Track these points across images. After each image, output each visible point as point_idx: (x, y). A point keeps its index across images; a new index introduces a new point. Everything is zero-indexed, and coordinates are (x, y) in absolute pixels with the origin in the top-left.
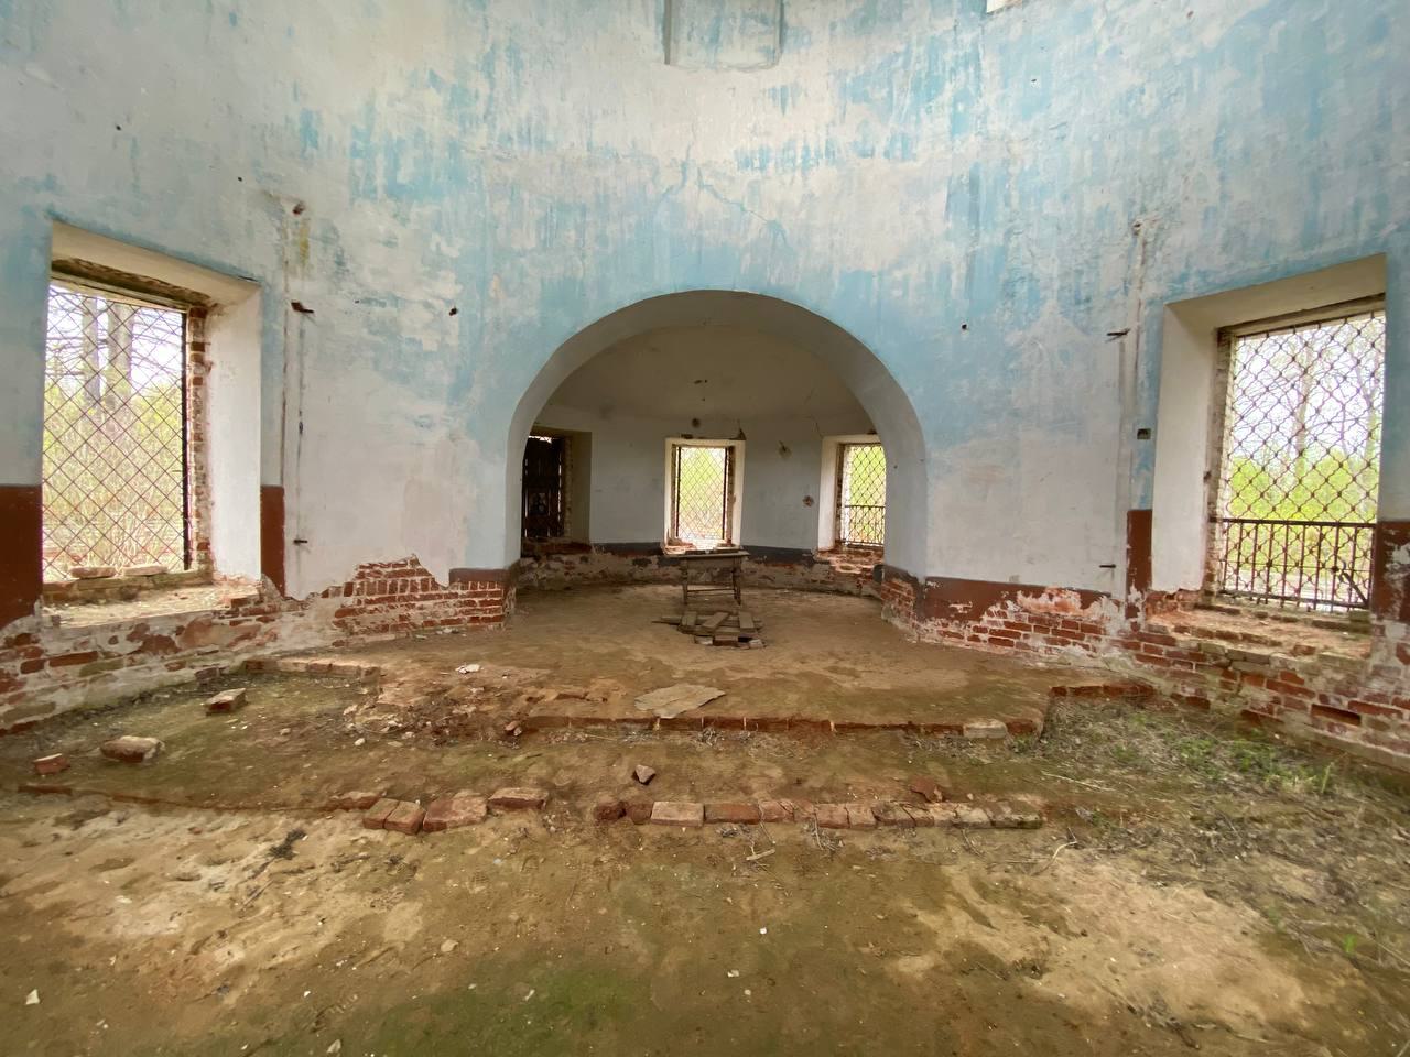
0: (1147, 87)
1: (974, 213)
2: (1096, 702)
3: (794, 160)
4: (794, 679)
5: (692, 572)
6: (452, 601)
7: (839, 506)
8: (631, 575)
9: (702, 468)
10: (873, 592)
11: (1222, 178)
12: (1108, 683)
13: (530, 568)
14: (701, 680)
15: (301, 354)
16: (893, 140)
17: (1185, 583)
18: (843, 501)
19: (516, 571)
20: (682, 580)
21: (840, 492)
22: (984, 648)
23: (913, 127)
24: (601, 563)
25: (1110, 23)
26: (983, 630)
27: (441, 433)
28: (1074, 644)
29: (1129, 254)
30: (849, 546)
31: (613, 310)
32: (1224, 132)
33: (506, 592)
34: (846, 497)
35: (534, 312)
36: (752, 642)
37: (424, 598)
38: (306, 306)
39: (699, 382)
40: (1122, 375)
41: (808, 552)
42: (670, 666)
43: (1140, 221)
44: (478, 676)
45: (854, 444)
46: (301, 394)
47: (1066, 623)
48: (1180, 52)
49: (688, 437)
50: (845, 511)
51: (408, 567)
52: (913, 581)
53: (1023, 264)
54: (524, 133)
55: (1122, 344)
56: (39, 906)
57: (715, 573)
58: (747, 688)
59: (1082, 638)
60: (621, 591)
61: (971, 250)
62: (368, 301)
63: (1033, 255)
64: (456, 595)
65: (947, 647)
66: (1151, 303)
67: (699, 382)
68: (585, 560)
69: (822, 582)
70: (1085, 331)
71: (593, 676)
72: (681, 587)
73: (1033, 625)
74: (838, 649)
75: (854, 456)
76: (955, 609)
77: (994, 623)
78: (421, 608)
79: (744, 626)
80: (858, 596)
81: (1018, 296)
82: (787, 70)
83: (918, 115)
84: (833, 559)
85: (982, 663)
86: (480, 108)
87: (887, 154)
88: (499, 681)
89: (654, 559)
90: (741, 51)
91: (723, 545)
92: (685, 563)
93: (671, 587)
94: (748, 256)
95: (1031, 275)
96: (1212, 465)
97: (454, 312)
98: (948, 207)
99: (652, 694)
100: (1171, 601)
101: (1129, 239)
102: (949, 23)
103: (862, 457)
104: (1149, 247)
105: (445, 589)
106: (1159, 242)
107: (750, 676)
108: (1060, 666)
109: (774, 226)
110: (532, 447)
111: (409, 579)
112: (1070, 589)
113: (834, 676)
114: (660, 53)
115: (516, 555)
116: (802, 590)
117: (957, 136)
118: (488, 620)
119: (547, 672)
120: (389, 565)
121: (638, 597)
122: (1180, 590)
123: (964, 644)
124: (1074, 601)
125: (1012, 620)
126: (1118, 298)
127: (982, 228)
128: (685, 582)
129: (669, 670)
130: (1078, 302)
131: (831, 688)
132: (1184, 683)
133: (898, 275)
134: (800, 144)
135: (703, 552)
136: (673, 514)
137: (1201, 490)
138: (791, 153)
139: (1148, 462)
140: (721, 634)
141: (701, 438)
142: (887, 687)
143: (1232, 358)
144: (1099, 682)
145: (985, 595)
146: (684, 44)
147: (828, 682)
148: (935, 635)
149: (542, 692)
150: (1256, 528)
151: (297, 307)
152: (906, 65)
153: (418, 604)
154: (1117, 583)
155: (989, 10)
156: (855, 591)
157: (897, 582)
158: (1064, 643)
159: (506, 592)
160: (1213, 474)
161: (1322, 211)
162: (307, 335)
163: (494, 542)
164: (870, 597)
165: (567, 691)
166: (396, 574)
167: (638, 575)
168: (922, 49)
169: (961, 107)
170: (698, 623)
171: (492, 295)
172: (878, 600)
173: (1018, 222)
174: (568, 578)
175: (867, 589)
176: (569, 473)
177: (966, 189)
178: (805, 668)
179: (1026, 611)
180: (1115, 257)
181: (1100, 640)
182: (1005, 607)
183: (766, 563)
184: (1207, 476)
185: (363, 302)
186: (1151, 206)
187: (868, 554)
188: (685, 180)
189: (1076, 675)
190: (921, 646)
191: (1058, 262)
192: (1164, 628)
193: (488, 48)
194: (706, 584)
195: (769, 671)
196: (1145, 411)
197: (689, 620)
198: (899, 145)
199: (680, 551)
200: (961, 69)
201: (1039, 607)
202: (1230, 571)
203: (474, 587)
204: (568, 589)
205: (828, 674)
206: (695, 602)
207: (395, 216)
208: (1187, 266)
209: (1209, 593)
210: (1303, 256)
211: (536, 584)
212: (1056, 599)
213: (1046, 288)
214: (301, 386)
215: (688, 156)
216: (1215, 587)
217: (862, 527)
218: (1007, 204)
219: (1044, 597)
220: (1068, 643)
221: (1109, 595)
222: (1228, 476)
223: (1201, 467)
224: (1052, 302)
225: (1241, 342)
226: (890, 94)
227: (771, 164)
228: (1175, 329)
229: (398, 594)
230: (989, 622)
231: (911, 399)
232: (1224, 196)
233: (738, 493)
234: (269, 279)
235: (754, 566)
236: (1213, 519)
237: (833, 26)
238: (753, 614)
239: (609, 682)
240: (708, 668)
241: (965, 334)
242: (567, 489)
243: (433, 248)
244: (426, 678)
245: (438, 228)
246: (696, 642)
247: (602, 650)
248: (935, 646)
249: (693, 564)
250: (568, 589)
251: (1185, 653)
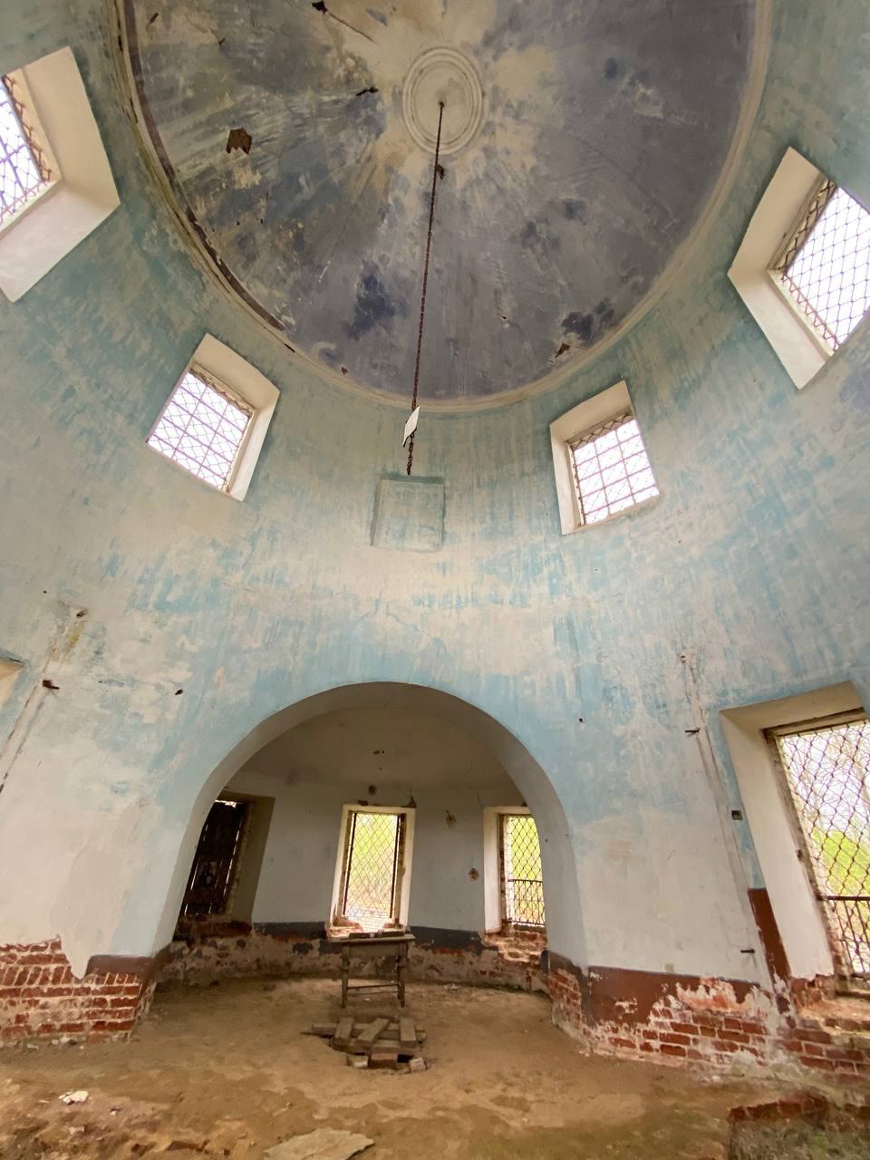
0: (665, 577)
1: (573, 642)
2: (778, 1124)
3: (451, 602)
4: (456, 1117)
5: (354, 962)
6: (80, 999)
7: (502, 880)
8: (288, 964)
9: (375, 833)
10: (544, 987)
11: (727, 631)
12: (784, 1099)
13: (180, 955)
14: (349, 1123)
15: (31, 723)
16: (515, 595)
17: (819, 968)
18: (506, 874)
19: (165, 956)
20: (342, 973)
21: (502, 864)
22: (657, 1058)
23: (525, 590)
24: (264, 949)
25: (635, 544)
26: (651, 1035)
27: (132, 798)
28: (742, 1048)
29: (683, 675)
30: (516, 927)
31: (311, 694)
32: (719, 604)
33: (144, 988)
34: (508, 868)
35: (246, 695)
36: (413, 1063)
37: (52, 993)
38: (55, 684)
39: (377, 752)
40: (705, 764)
41: (476, 934)
42: (313, 1102)
43: (684, 654)
44: (83, 1109)
45: (512, 815)
46: (15, 758)
47: (729, 1022)
48: (680, 559)
49: (364, 803)
50: (509, 885)
51: (47, 952)
52: (576, 971)
53: (614, 677)
54: (269, 577)
55: (698, 739)
56: (580, 702)
57: (380, 963)
58: (402, 1134)
59: (746, 1040)
60: (274, 988)
61: (575, 666)
62: (110, 682)
63: (619, 672)
64: (87, 991)
65: (621, 1061)
66: (708, 710)
67: (377, 752)
68: (241, 944)
69: (492, 973)
70: (668, 727)
71: (218, 1116)
72: (340, 983)
73: (699, 1026)
74: (507, 1071)
75: (512, 826)
76: (620, 1008)
77: (661, 1025)
78: (43, 1007)
79: (405, 1037)
80: (528, 991)
81: (614, 700)
82: (445, 555)
83: (528, 582)
84: (501, 943)
85: (657, 1081)
86: (242, 560)
87: (511, 603)
88: (105, 1118)
89: (316, 943)
90: (419, 542)
91: (390, 926)
92: (346, 950)
93: (330, 982)
94: (419, 660)
95: (621, 685)
96: (799, 843)
97: (179, 692)
98: (555, 637)
99: (285, 1145)
100: (813, 990)
101: (680, 665)
102: (541, 538)
103: (519, 827)
104: (695, 671)
105: (78, 981)
106: (701, 669)
107: (405, 1114)
108: (735, 1079)
109: (438, 641)
110: (217, 810)
111: (43, 967)
112: (723, 980)
113: (501, 1110)
114: (368, 540)
115: (167, 939)
116: (470, 985)
117: (554, 596)
118: (114, 1027)
119: (165, 1107)
120: (27, 948)
121: (292, 996)
122: (817, 976)
123: (637, 1055)
124: (729, 994)
125: (678, 1021)
126: (685, 705)
127: (580, 652)
128: (345, 975)
129: (311, 1107)
130: (658, 707)
131: (497, 1130)
132: (852, 1090)
133: (527, 679)
134: (455, 595)
135: (367, 935)
136: (342, 887)
137: (799, 867)
138: (449, 599)
139: (747, 841)
140: (380, 1050)
141: (376, 805)
142: (560, 1124)
143: (780, 752)
144: (772, 1098)
145: (651, 987)
146: (383, 536)
147: (494, 1119)
148: (607, 1044)
149: (153, 1138)
150: (856, 905)
151: (47, 684)
152: (518, 556)
153: (42, 1000)
154: (757, 970)
155: (563, 533)
156: (525, 985)
157: (563, 972)
158: (733, 1048)
159: (144, 988)
160: (803, 851)
161: (799, 652)
162: (44, 708)
163: (144, 926)
164: (540, 993)
165: (183, 1138)
166: (31, 960)
167: (295, 966)
168: (527, 550)
169: (554, 581)
170: (354, 1034)
171: (216, 680)
172: (548, 996)
173: (603, 650)
174: (218, 968)
175: (537, 983)
176: (245, 839)
177: (565, 627)
178: (470, 1099)
179: (689, 1008)
180: (676, 676)
181: (763, 1041)
182: (668, 1003)
183: (434, 948)
184: (800, 855)
185: (106, 682)
186: (687, 645)
187: (533, 938)
188: (377, 610)
189: (751, 1090)
190: (595, 1059)
191: (637, 678)
192: (816, 1022)
193: (256, 529)
194: (369, 977)
195: (429, 1106)
196: (731, 795)
197: (343, 1031)
198: (518, 598)
199: (343, 933)
200: (551, 561)
201: (699, 1003)
202: (853, 954)
203: (110, 981)
204: (215, 983)
205: (496, 1108)
206: (354, 1004)
207: (156, 622)
208: (724, 684)
209: (843, 978)
210: (797, 681)
211: (181, 977)
212: (713, 992)
213: (633, 695)
214: (19, 750)
215: (380, 596)
216: (845, 970)
217: (526, 908)
218: (595, 638)
219: (701, 991)
220: (736, 1048)
221: (758, 986)
222: (817, 854)
223: (793, 849)
224: (639, 706)
225: (783, 740)
226: (511, 571)
227: (436, 605)
228: (730, 728)
229: (25, 986)
230: (657, 1023)
231: (550, 777)
232: (733, 642)
233: (408, 864)
234: (34, 661)
235: (422, 953)
236: (819, 898)
237: (473, 535)
238: (416, 1019)
239: (236, 1125)
240: (356, 1103)
241: (582, 726)
242: (240, 858)
243: (178, 644)
244: (20, 1109)
245: (186, 632)
246: (349, 1063)
247: (234, 1075)
248: (608, 1060)
249: (356, 951)
250: (215, 983)
251: (842, 1050)
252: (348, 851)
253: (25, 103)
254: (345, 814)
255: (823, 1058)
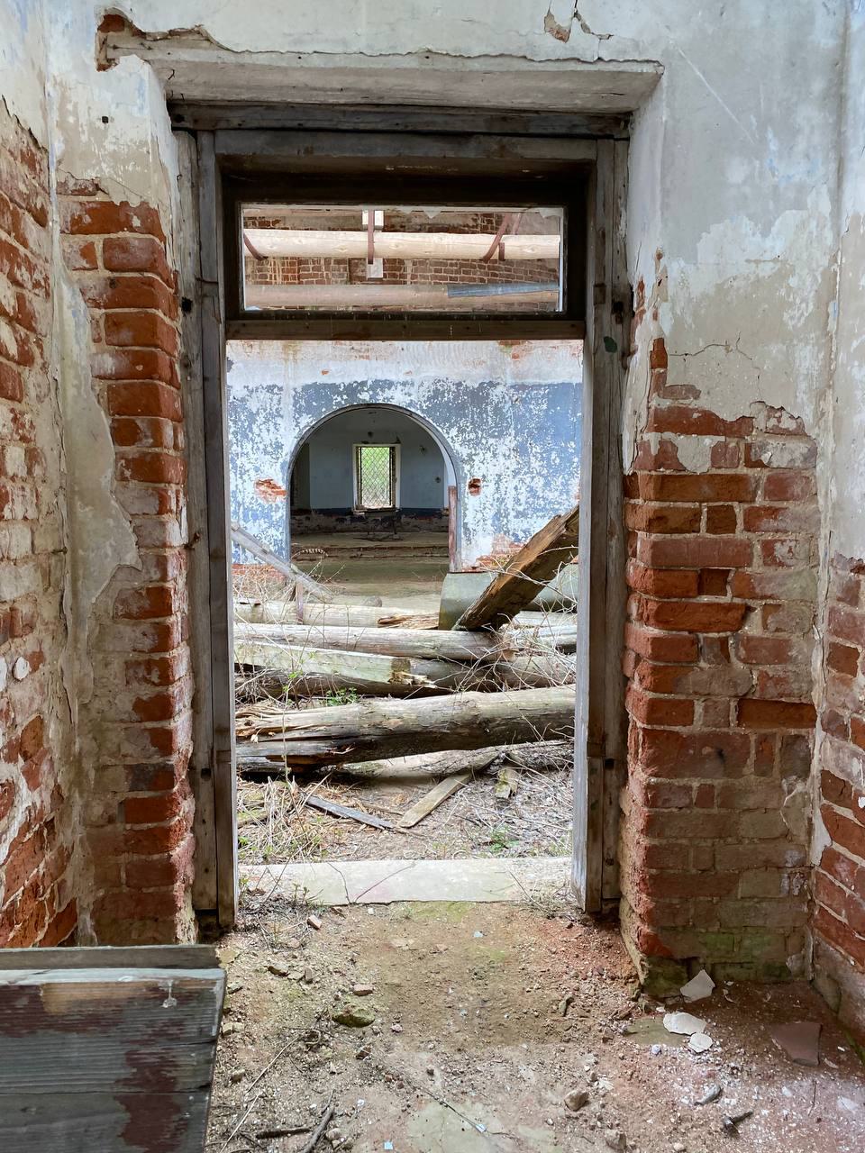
68: (308, 519)
89: (348, 517)
167: (339, 528)
233: (398, 476)
235: (409, 520)
252: (359, 469)
253: (655, 256)
254: (354, 449)
255: (839, 918)
